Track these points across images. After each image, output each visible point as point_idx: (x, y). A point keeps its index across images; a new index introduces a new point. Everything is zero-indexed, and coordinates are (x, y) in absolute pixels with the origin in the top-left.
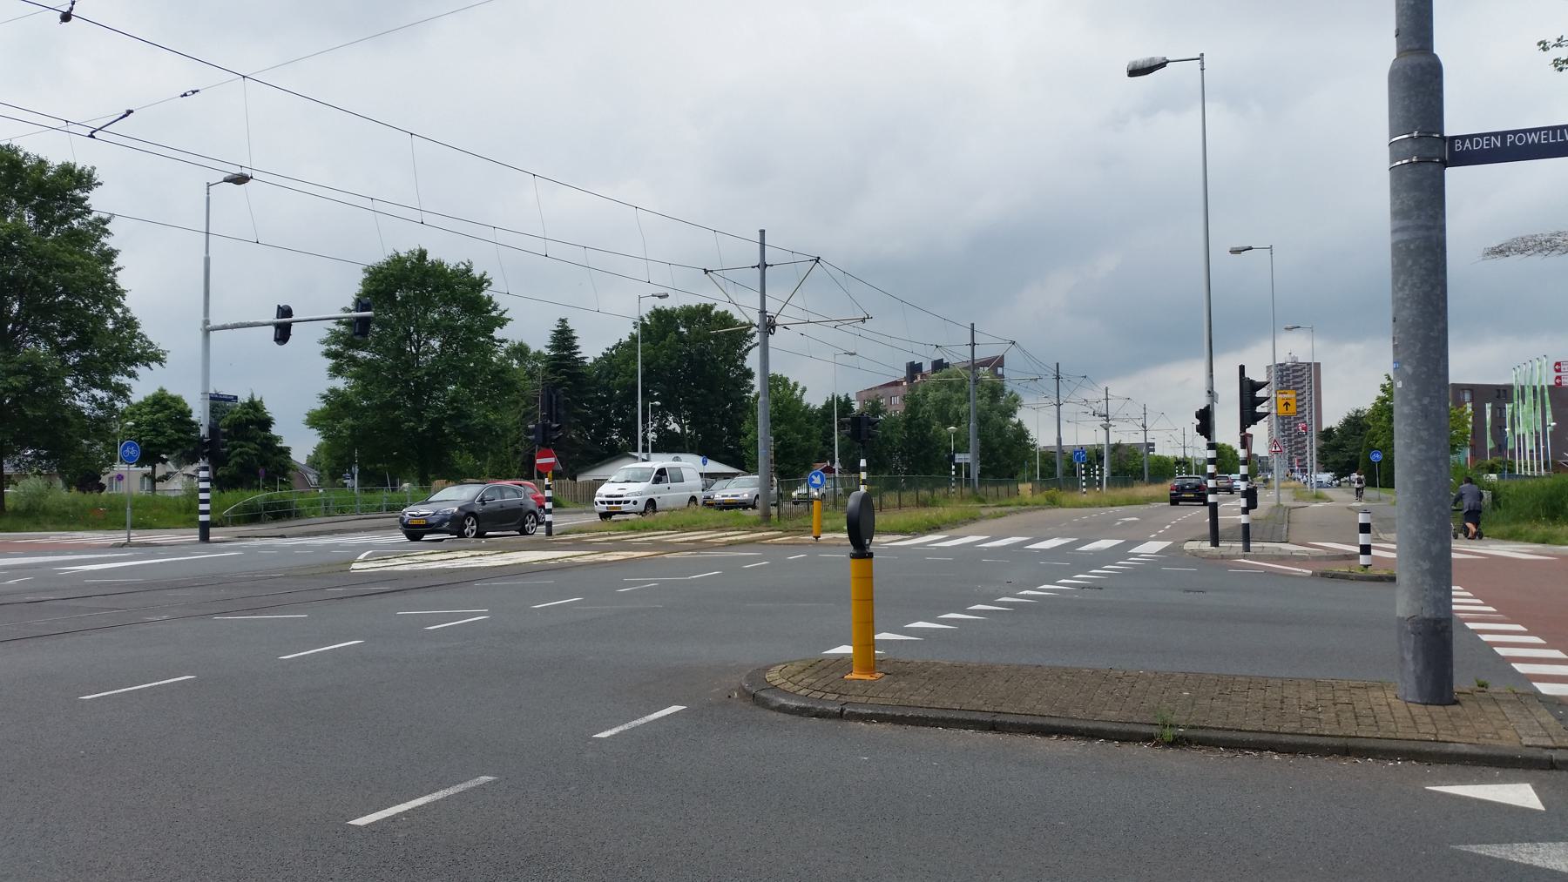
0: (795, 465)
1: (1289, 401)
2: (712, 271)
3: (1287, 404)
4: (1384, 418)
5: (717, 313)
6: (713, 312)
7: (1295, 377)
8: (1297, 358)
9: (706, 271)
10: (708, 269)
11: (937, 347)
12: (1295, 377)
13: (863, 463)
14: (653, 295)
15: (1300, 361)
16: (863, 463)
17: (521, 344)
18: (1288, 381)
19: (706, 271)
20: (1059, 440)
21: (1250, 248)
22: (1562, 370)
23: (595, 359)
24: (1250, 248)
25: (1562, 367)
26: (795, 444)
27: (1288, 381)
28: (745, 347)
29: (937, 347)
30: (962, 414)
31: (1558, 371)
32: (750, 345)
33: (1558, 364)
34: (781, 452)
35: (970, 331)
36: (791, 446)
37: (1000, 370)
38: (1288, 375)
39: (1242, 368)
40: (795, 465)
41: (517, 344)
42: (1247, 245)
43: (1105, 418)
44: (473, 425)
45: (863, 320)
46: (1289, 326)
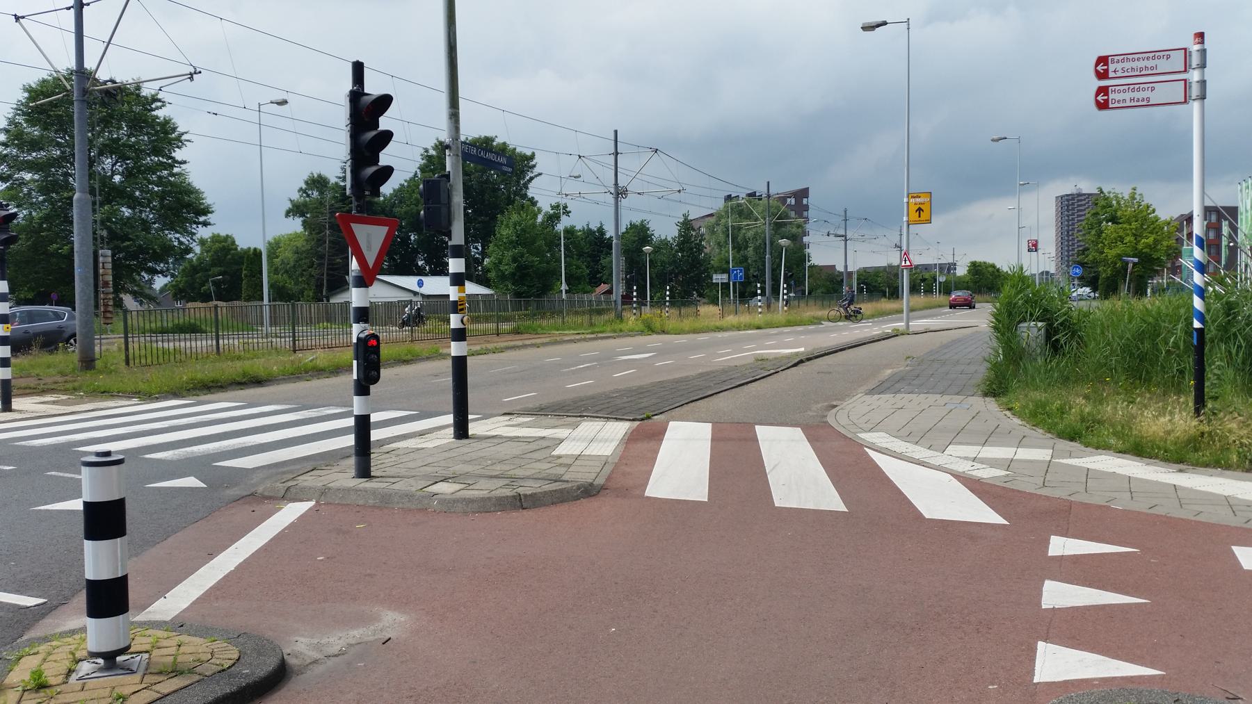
0: (531, 287)
1: (922, 207)
2: (23, 17)
3: (920, 210)
4: (1093, 232)
5: (498, 144)
6: (495, 144)
7: (1079, 206)
8: (1081, 189)
9: (17, 18)
10: (19, 14)
11: (580, 157)
12: (1079, 206)
13: (635, 288)
14: (272, 103)
15: (1084, 192)
16: (635, 288)
17: (320, 176)
18: (1073, 209)
19: (17, 18)
20: (846, 267)
21: (885, 23)
22: (1111, 75)
23: (394, 190)
24: (885, 23)
25: (1112, 67)
26: (532, 266)
27: (1073, 209)
28: (528, 178)
29: (580, 157)
30: (749, 239)
31: (1102, 75)
32: (532, 175)
33: (1103, 60)
34: (518, 274)
35: (613, 142)
36: (526, 267)
37: (805, 201)
38: (1073, 204)
39: (358, 69)
40: (531, 287)
41: (316, 176)
42: (880, 19)
43: (843, 238)
44: (1040, 284)
45: (191, 77)
46: (995, 137)
